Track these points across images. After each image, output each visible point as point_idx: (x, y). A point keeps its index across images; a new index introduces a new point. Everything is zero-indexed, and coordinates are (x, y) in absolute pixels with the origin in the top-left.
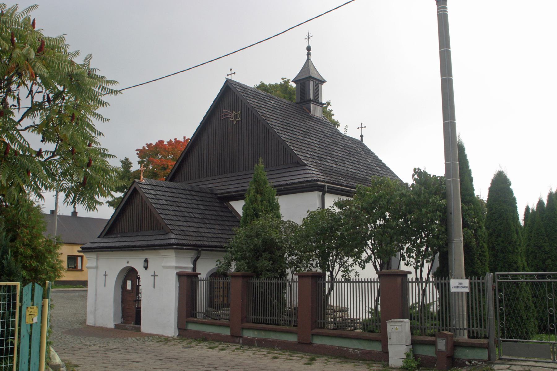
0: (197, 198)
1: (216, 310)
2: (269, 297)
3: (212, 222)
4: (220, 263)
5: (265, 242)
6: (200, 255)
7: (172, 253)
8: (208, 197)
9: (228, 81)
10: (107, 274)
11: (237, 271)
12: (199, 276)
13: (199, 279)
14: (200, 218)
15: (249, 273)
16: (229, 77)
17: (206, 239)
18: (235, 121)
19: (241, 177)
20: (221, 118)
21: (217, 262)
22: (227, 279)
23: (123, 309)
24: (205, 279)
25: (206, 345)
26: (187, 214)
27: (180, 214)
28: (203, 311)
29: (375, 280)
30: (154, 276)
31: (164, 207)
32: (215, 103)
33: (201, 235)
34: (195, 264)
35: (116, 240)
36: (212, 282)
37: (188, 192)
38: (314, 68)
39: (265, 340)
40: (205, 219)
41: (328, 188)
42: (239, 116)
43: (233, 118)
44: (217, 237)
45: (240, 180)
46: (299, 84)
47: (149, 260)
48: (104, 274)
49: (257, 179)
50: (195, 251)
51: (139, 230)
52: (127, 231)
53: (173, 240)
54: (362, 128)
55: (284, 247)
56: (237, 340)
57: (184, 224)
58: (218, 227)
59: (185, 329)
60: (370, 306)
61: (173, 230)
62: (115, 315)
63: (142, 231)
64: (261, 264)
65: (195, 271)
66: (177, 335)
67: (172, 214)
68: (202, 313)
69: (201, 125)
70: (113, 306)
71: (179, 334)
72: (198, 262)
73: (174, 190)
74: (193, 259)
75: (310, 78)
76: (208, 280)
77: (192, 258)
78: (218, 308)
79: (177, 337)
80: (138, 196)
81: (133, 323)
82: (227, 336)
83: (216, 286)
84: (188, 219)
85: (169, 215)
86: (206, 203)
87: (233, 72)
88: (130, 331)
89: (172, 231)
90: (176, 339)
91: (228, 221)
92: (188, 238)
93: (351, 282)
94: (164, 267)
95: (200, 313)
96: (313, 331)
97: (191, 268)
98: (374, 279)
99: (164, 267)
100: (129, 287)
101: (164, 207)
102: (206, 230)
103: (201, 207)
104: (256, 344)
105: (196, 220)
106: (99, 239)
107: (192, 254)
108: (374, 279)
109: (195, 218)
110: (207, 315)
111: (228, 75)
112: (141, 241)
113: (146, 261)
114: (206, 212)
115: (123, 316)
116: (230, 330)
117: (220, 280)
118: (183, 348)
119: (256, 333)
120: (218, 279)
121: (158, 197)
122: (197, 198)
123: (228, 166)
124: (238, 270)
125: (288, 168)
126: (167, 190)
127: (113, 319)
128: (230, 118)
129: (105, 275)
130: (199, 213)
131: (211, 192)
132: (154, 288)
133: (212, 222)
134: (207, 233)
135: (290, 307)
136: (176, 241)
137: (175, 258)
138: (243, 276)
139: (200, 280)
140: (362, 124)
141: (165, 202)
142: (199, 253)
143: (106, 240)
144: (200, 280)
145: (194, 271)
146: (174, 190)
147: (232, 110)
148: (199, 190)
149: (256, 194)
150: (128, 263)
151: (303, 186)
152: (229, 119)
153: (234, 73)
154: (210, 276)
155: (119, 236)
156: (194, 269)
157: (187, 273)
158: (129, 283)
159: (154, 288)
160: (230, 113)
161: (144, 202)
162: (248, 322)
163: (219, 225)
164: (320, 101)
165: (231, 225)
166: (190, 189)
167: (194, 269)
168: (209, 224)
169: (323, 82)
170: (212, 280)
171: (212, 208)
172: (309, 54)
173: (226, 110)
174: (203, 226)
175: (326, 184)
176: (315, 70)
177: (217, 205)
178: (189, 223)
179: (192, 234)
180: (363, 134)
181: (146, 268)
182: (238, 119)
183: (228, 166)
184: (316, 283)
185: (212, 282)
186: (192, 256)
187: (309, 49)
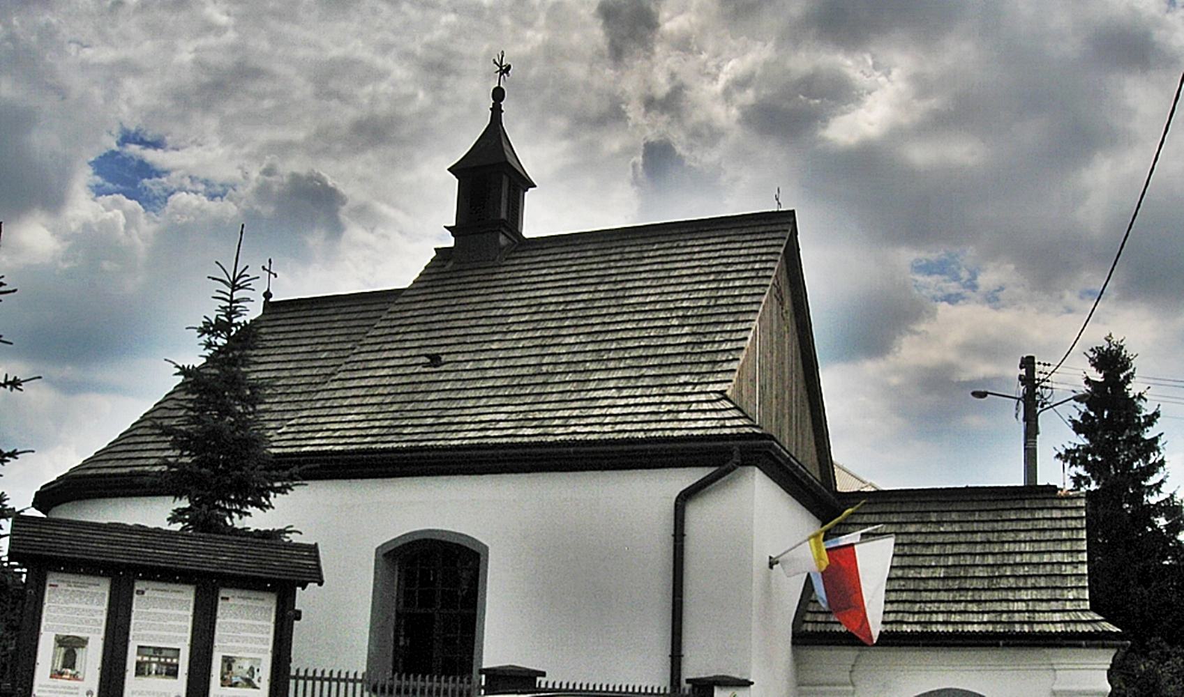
172: (496, 111)
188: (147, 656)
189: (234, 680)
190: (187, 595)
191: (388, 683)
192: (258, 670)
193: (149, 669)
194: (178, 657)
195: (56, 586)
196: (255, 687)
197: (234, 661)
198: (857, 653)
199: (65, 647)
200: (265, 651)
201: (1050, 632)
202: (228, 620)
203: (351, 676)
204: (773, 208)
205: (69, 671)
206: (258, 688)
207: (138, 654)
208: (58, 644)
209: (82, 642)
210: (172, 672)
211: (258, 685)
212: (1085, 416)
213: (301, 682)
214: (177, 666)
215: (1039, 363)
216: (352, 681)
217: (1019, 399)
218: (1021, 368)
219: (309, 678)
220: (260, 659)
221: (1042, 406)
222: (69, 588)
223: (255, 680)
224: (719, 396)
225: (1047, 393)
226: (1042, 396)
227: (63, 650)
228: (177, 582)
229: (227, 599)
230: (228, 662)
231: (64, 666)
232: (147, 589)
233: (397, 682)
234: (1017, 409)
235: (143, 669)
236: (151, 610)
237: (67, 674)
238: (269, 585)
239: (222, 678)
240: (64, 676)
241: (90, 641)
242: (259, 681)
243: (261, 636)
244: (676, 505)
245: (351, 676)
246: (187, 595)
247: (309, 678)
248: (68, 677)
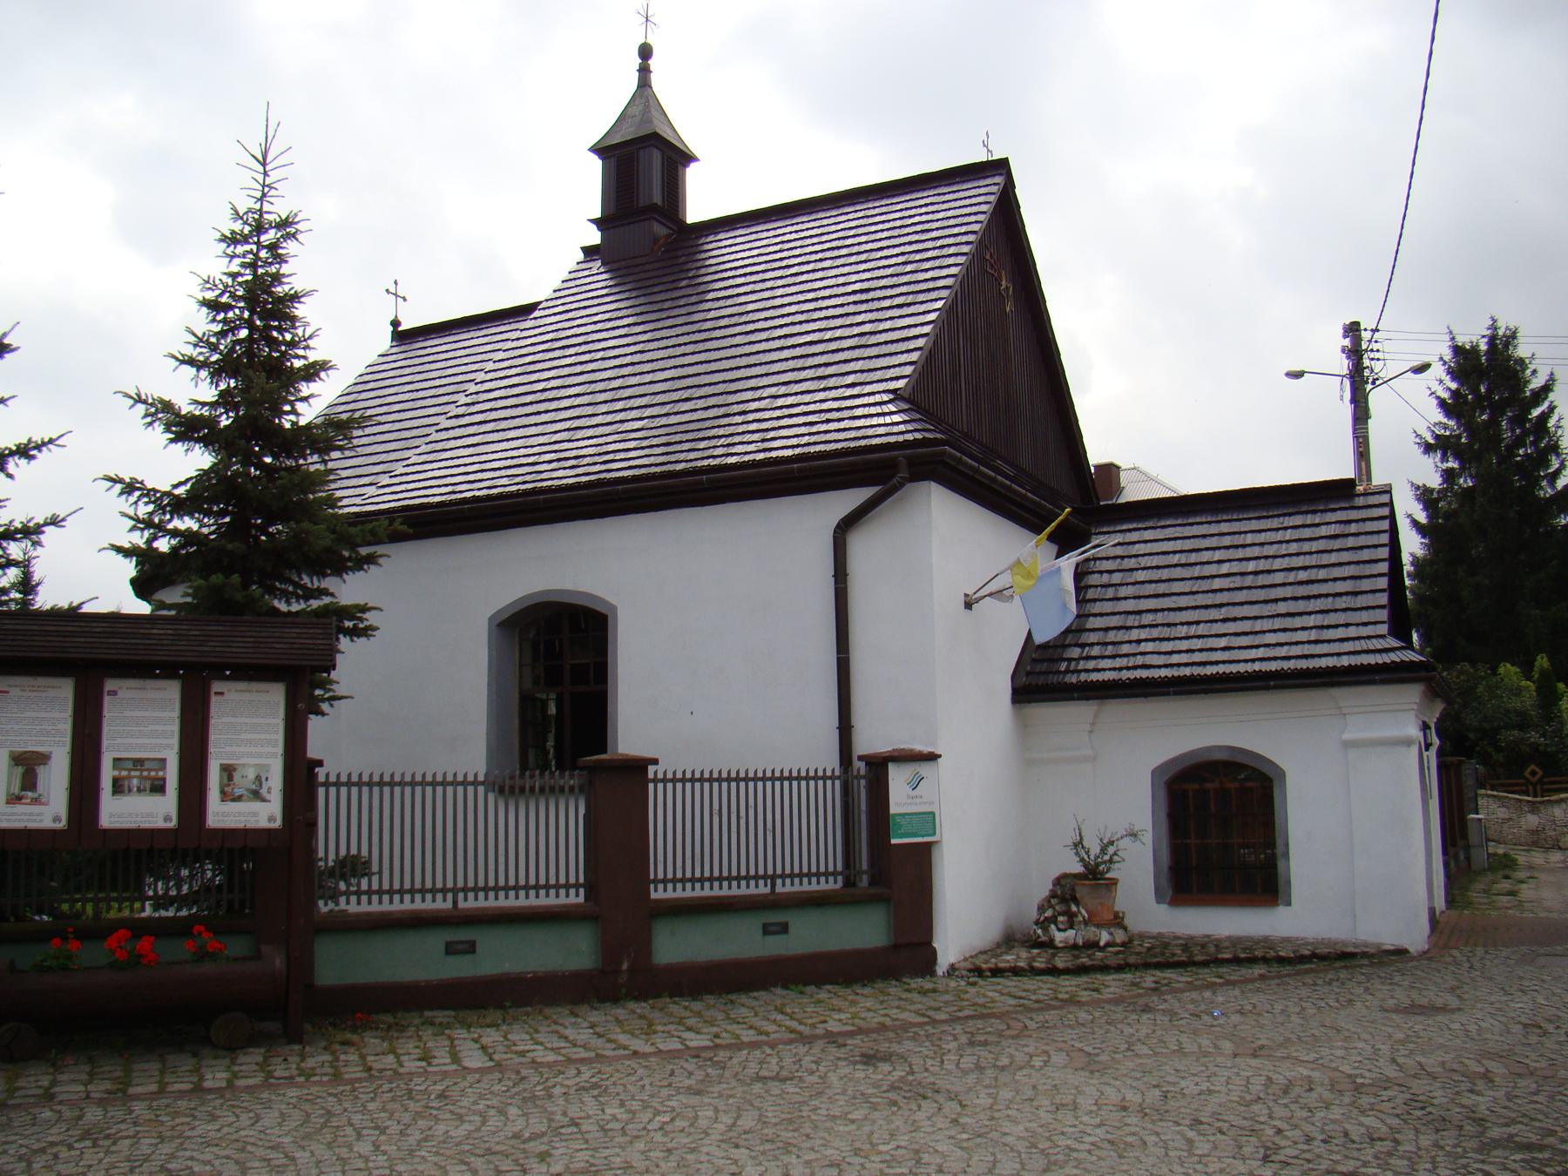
169: (687, 158)
172: (644, 71)
187: (645, 52)
188: (125, 770)
189: (238, 792)
190: (170, 692)
191: (507, 782)
192: (267, 779)
193: (129, 787)
194: (164, 768)
195: (7, 692)
196: (264, 800)
197: (235, 770)
198: (1095, 708)
199: (22, 765)
200: (274, 755)
201: (1393, 662)
202: (224, 720)
203: (724, 775)
204: (981, 157)
205: (30, 794)
206: (269, 801)
207: (115, 768)
208: (13, 763)
209: (44, 758)
210: (159, 788)
211: (267, 796)
212: (1455, 394)
213: (670, 786)
214: (164, 780)
215: (1365, 330)
216: (821, 778)
217: (1344, 376)
218: (1345, 337)
219: (354, 784)
220: (269, 765)
221: (1373, 383)
222: (24, 694)
223: (264, 791)
224: (891, 396)
225: (1377, 366)
226: (1372, 371)
227: (20, 770)
228: (157, 677)
229: (222, 694)
230: (228, 771)
231: (24, 788)
232: (120, 688)
233: (518, 782)
234: (1341, 389)
235: (122, 786)
236: (28, 714)
237: (27, 798)
238: (228, 673)
239: (223, 792)
240: (23, 801)
241: (53, 756)
242: (269, 792)
243: (268, 736)
244: (835, 538)
245: (820, 773)
246: (170, 692)
247: (354, 784)
248: (29, 801)
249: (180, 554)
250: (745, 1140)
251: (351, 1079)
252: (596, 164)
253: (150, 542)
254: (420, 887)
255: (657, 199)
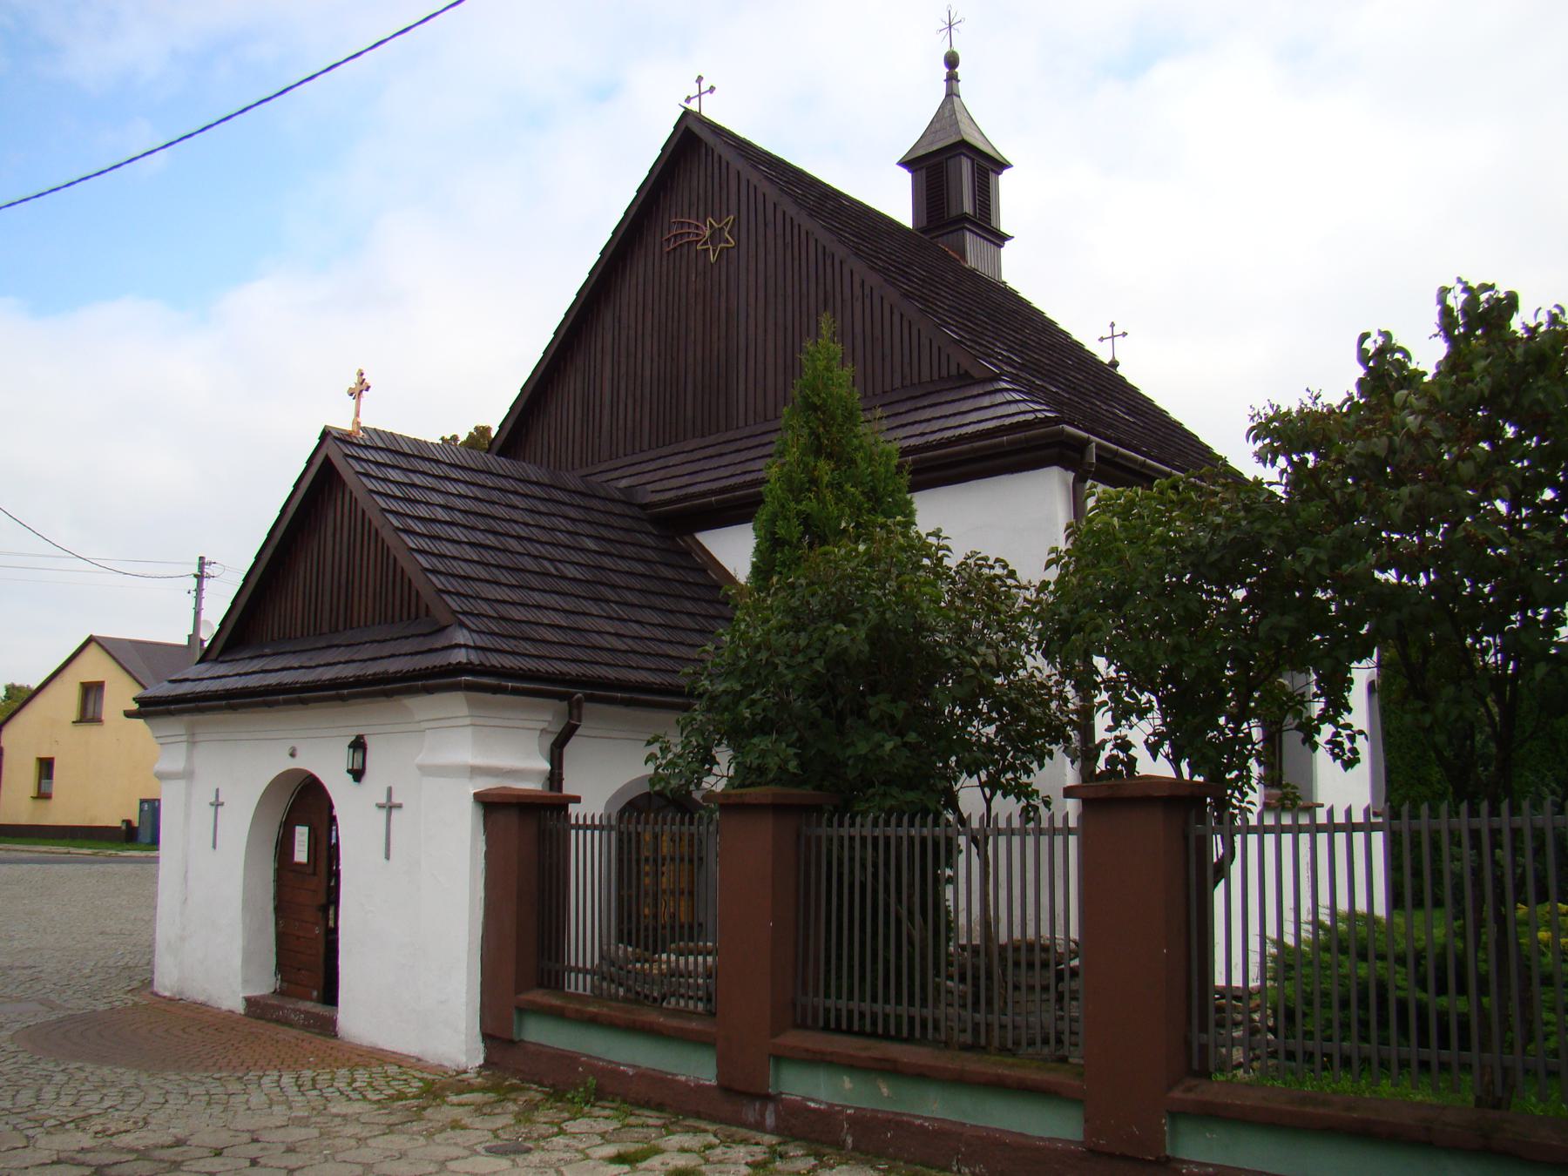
0: (572, 513)
1: (647, 954)
2: (887, 906)
3: (630, 597)
4: (665, 750)
5: (878, 636)
6: (580, 721)
7: (454, 705)
8: (615, 514)
9: (687, 114)
10: (221, 800)
11: (742, 786)
12: (573, 809)
13: (573, 821)
14: (580, 580)
15: (805, 793)
16: (693, 106)
17: (606, 657)
18: (714, 251)
19: (738, 445)
20: (665, 244)
21: (649, 743)
22: (701, 818)
23: (282, 939)
24: (597, 822)
25: (603, 1135)
26: (530, 564)
27: (503, 559)
28: (581, 965)
29: (1358, 817)
30: (390, 807)
31: (437, 529)
32: (643, 195)
33: (583, 642)
34: (556, 757)
35: (257, 665)
36: (629, 834)
37: (538, 491)
38: (969, 121)
39: (899, 1123)
40: (602, 584)
41: (1098, 457)
42: (729, 233)
43: (705, 243)
44: (649, 654)
45: (733, 455)
46: (924, 171)
47: (369, 741)
48: (213, 799)
49: (816, 400)
50: (556, 702)
51: (341, 627)
52: (299, 634)
53: (463, 651)
54: (1113, 337)
55: (973, 665)
56: (751, 1115)
57: (515, 596)
58: (657, 618)
59: (512, 1042)
60: (1271, 932)
61: (465, 613)
62: (247, 960)
63: (352, 628)
64: (863, 748)
65: (560, 789)
66: (480, 1060)
67: (468, 557)
68: (585, 971)
69: (594, 278)
70: (239, 927)
71: (486, 1060)
72: (569, 750)
73: (481, 479)
74: (552, 738)
75: (963, 147)
76: (611, 828)
77: (543, 730)
78: (655, 945)
79: (479, 1074)
80: (340, 495)
81: (315, 994)
82: (700, 1089)
83: (646, 852)
84: (535, 581)
85: (455, 558)
86: (605, 533)
87: (705, 87)
88: (295, 1032)
89: (460, 616)
90: (471, 1088)
91: (693, 599)
92: (529, 648)
93: (1319, 828)
94: (427, 771)
95: (578, 970)
96: (1177, 1093)
97: (540, 773)
98: (1348, 812)
99: (427, 771)
100: (301, 854)
101: (437, 529)
102: (608, 626)
103: (590, 544)
104: (849, 1140)
105: (565, 586)
106: (203, 666)
107: (544, 718)
108: (1348, 812)
109: (564, 578)
110: (608, 971)
111: (688, 100)
112: (340, 663)
113: (359, 745)
114: (607, 562)
115: (281, 967)
116: (714, 1063)
117: (658, 828)
118: (491, 1151)
119: (847, 1082)
120: (656, 823)
121: (415, 494)
122: (572, 513)
123: (690, 414)
124: (746, 775)
125: (924, 395)
126: (454, 474)
127: (239, 979)
128: (697, 242)
129: (217, 804)
130: (578, 564)
131: (627, 499)
132: (388, 857)
133: (630, 597)
134: (606, 636)
135: (976, 941)
136: (475, 657)
137: (469, 730)
138: (778, 809)
139: (578, 827)
140: (1112, 325)
141: (441, 514)
142: (575, 712)
143: (221, 669)
144: (578, 827)
145: (551, 789)
146: (481, 479)
147: (702, 214)
148: (582, 488)
149: (811, 460)
150: (293, 755)
151: (1001, 445)
152: (693, 249)
153: (712, 89)
154: (622, 812)
155: (267, 651)
156: (555, 778)
157: (519, 796)
158: (302, 834)
159: (388, 857)
160: (697, 227)
161: (360, 514)
162: (802, 1025)
163: (660, 610)
164: (993, 224)
165: (703, 612)
166: (547, 481)
167: (555, 778)
168: (616, 603)
169: (1001, 165)
170: (632, 828)
171: (629, 551)
172: (952, 78)
173: (682, 217)
174: (593, 608)
175: (1092, 437)
176: (973, 126)
177: (650, 541)
178: (535, 595)
179: (549, 635)
180: (1117, 358)
181: (358, 774)
182: (727, 241)
183: (690, 414)
184: (1186, 838)
185: (629, 834)
186: (545, 725)
187: (952, 61)
249: (1563, 483)
250: (226, 1164)
251: (567, 1060)
252: (906, 177)
253: (1335, 489)
254: (1301, 836)
255: (968, 207)
